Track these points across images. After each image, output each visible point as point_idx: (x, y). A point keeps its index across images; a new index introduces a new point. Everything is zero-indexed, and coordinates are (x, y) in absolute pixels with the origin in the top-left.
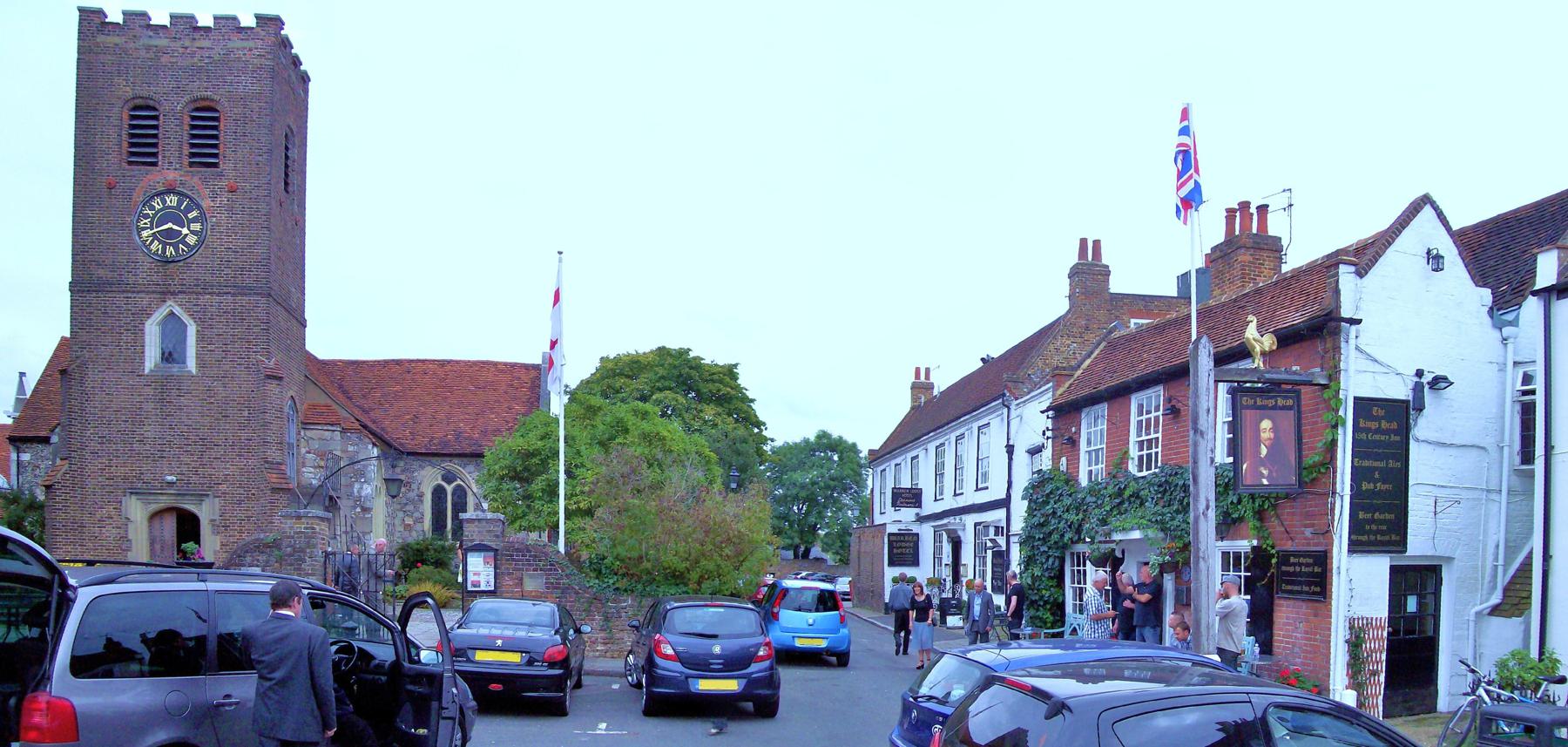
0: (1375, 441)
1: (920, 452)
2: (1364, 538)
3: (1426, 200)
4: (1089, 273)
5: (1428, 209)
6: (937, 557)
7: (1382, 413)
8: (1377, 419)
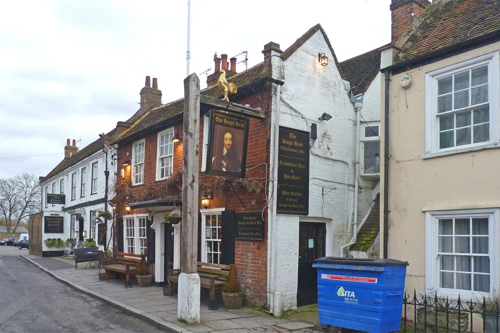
0: (291, 152)
1: (65, 177)
2: (286, 206)
3: (318, 28)
4: (150, 92)
5: (319, 31)
6: (72, 227)
7: (295, 137)
8: (292, 140)
